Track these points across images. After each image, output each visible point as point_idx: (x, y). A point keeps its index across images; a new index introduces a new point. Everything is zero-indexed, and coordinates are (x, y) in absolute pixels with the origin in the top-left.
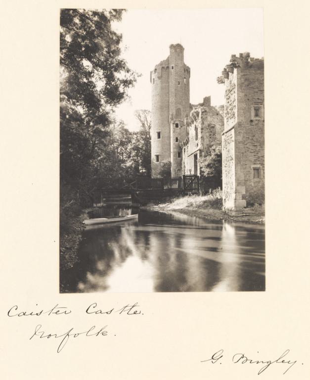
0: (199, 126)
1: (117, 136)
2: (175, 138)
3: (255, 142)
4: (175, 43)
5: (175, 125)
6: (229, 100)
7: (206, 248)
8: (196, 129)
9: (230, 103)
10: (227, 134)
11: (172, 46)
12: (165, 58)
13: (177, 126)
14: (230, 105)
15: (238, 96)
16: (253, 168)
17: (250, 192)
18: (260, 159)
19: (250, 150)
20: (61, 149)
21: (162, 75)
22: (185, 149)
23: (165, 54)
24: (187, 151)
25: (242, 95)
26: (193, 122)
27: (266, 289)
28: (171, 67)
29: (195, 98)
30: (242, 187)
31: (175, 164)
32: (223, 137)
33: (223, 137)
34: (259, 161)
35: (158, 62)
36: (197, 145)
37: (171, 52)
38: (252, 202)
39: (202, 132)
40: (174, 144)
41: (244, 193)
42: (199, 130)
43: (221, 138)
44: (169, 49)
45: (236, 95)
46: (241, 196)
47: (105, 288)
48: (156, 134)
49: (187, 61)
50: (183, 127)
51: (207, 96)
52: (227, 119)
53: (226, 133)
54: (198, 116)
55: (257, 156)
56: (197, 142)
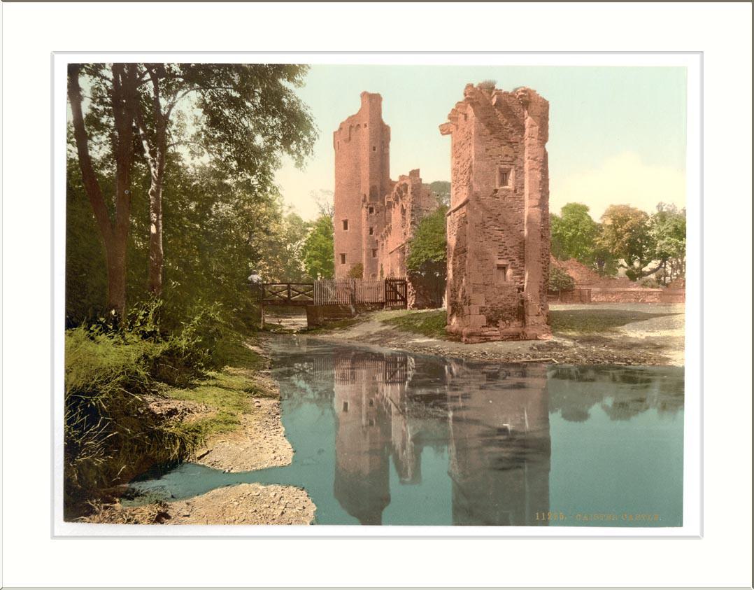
1: (285, 226)
3: (501, 224)
4: (371, 91)
5: (368, 210)
6: (460, 160)
8: (403, 211)
9: (461, 163)
10: (457, 212)
12: (355, 112)
14: (462, 166)
16: (498, 265)
17: (493, 302)
18: (508, 252)
23: (353, 106)
25: (482, 149)
26: (397, 200)
27: (67, 523)
35: (344, 118)
36: (405, 234)
37: (362, 103)
39: (412, 215)
42: (408, 212)
43: (446, 219)
44: (360, 98)
46: (478, 310)
47: (444, 130)
48: (342, 224)
49: (387, 118)
51: (415, 169)
52: (456, 189)
53: (454, 211)
54: (406, 190)
56: (403, 230)
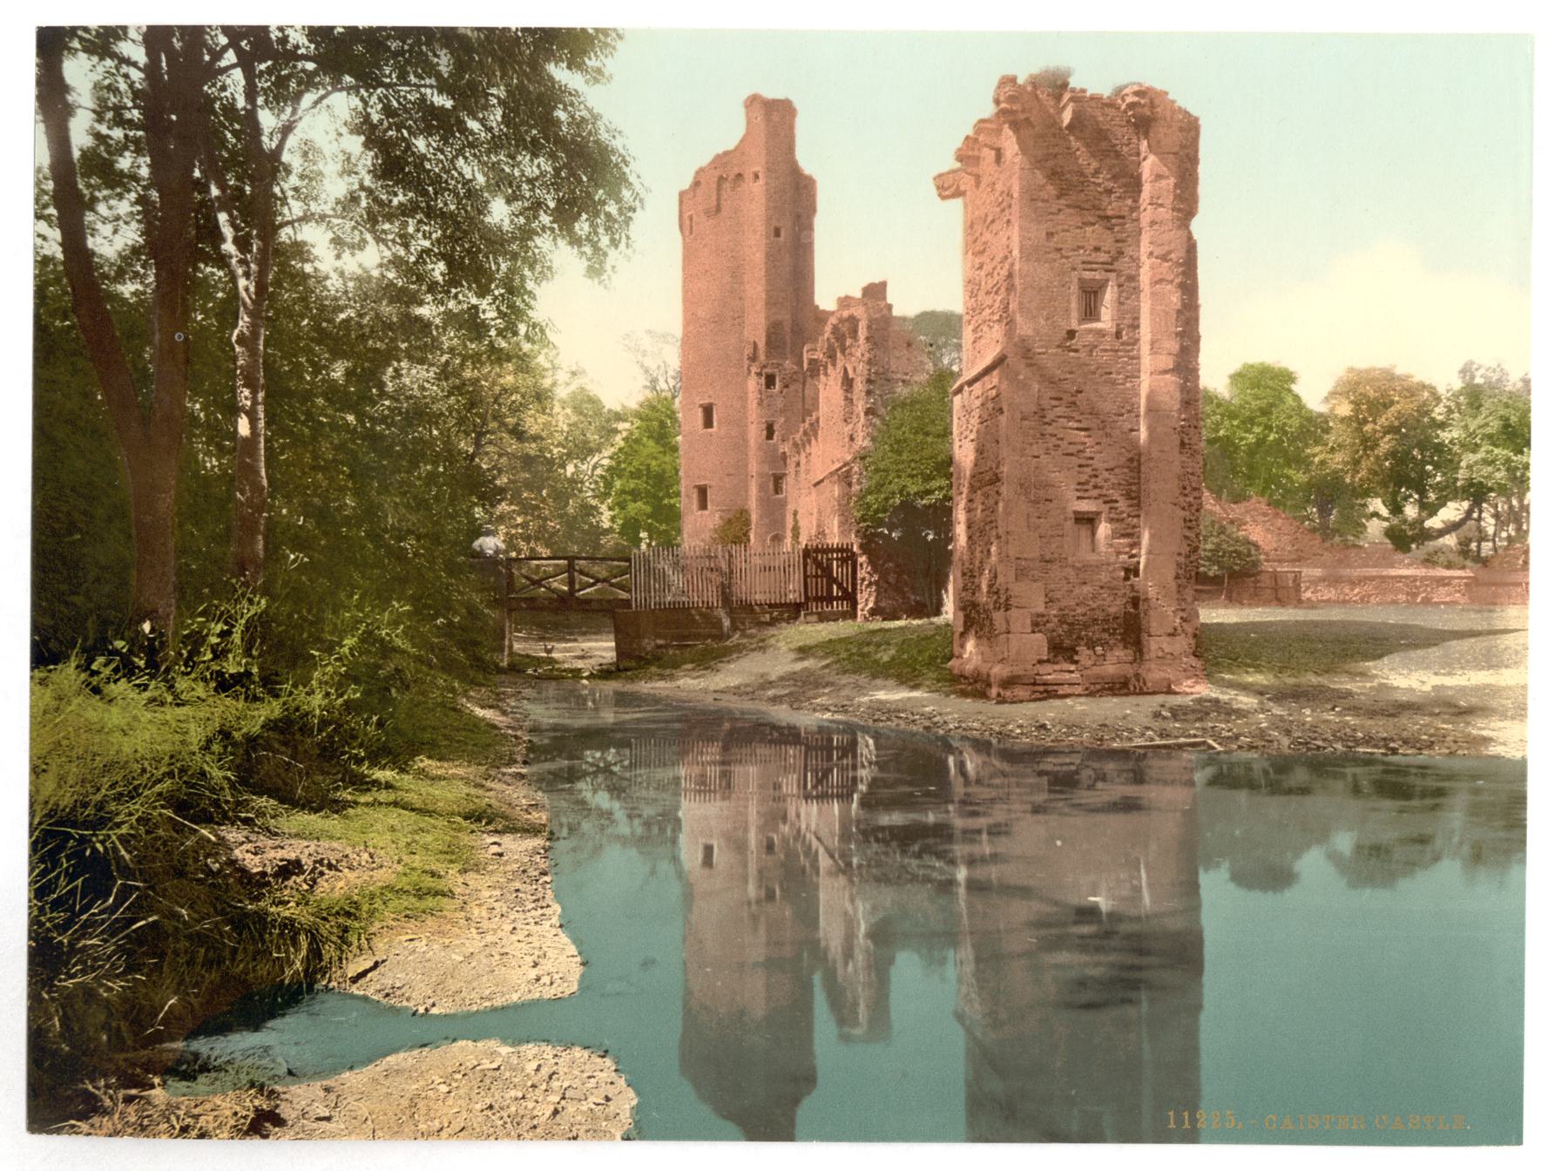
0: (859, 371)
2: (764, 426)
4: (770, 93)
5: (763, 380)
6: (984, 258)
7: (1006, 861)
8: (848, 383)
10: (977, 385)
11: (753, 102)
12: (731, 145)
13: (770, 381)
14: (990, 274)
15: (1023, 238)
16: (1076, 512)
18: (1099, 481)
19: (1064, 444)
20: (1170, 1141)
21: (718, 200)
22: (798, 464)
24: (807, 472)
25: (1038, 232)
26: (832, 357)
28: (748, 176)
29: (826, 296)
30: (1035, 585)
31: (761, 517)
32: (957, 400)
33: (957, 400)
34: (1095, 487)
36: (852, 439)
38: (1067, 643)
39: (869, 393)
40: (760, 448)
41: (1041, 609)
42: (859, 386)
44: (743, 110)
45: (1015, 233)
46: (1028, 621)
50: (792, 388)
51: (877, 281)
52: (975, 331)
53: (970, 383)
54: (854, 332)
55: (1088, 470)
